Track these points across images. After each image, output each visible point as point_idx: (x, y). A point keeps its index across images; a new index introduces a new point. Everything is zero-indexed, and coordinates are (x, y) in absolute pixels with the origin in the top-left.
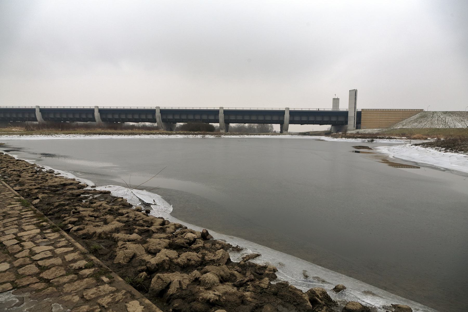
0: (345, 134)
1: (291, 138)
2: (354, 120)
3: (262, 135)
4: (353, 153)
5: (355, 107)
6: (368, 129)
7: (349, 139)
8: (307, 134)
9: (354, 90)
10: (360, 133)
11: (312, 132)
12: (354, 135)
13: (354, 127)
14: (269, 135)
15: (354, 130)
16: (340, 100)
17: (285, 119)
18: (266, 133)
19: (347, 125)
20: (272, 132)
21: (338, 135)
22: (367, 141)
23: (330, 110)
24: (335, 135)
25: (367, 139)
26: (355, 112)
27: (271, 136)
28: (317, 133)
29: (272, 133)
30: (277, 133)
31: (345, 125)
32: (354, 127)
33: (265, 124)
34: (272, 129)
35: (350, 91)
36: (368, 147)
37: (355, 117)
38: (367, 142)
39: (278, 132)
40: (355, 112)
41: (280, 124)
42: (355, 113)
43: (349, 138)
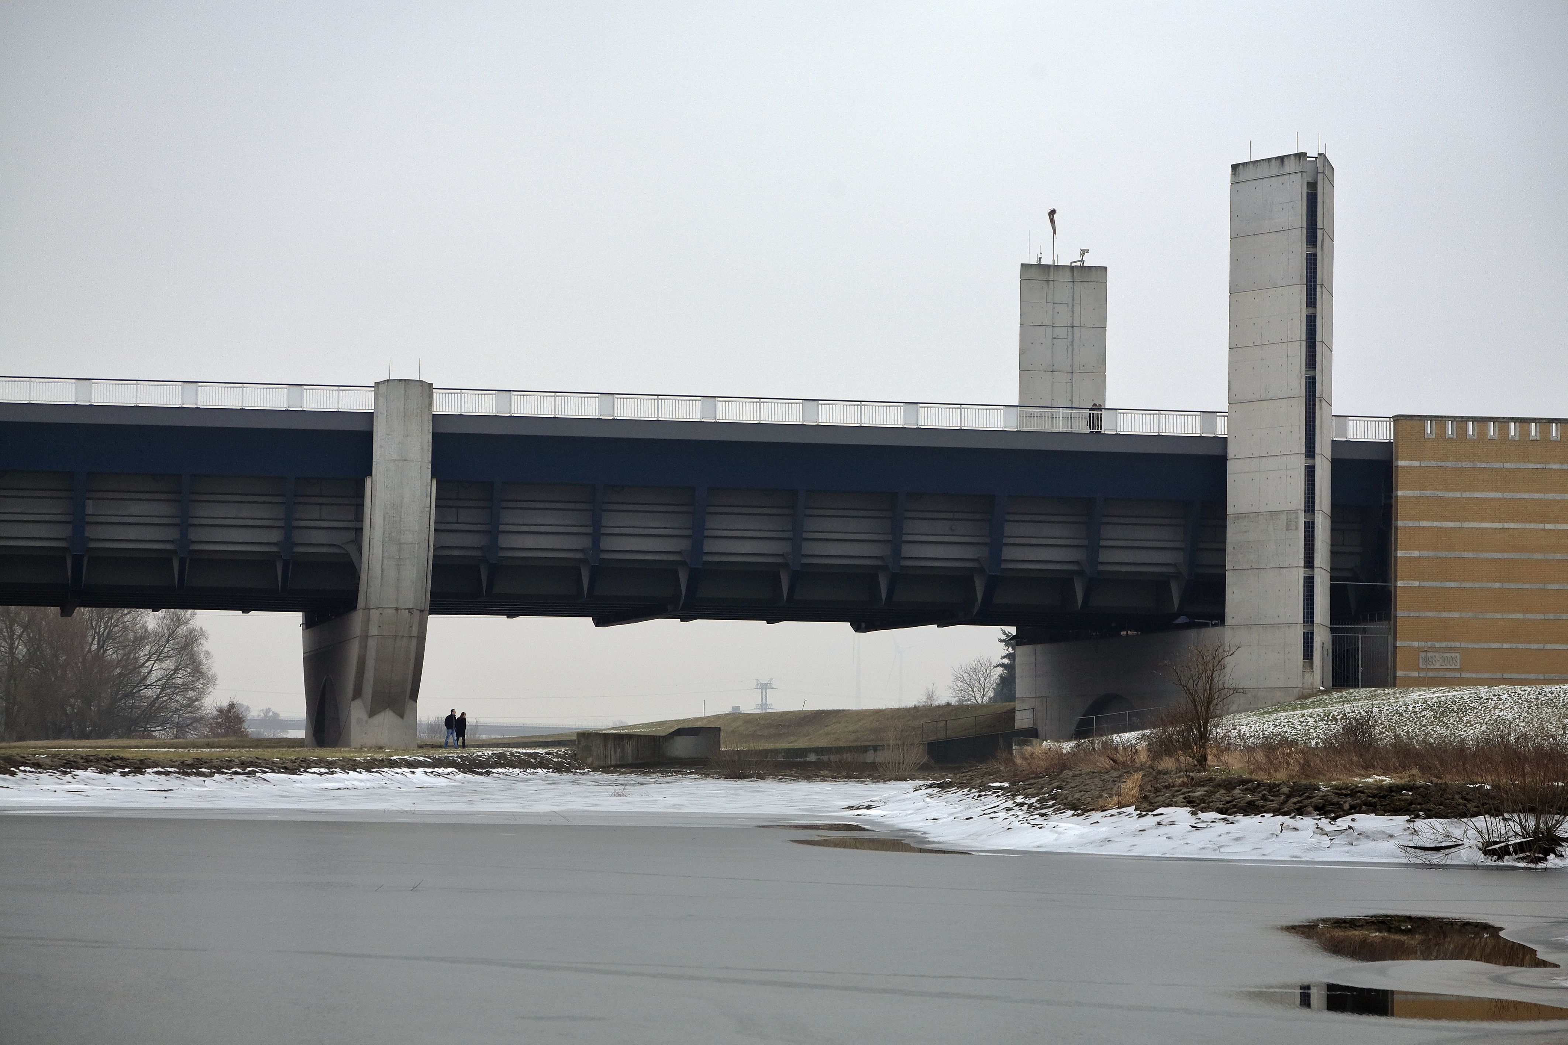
0: (1186, 747)
1: (459, 806)
2: (1309, 562)
3: (38, 766)
4: (1305, 1012)
5: (1311, 384)
6: (1483, 691)
7: (1246, 823)
8: (681, 748)
9: (1291, 166)
10: (1383, 736)
11: (750, 720)
12: (1306, 766)
13: (1308, 654)
14: (138, 767)
15: (1304, 697)
16: (1111, 277)
17: (378, 534)
18: (102, 746)
19: (1210, 633)
20: (181, 728)
21: (1104, 762)
22: (1468, 854)
23: (993, 421)
24: (1062, 763)
25: (1480, 822)
26: (1310, 451)
27: (172, 782)
28: (822, 743)
29: (192, 736)
30: (259, 743)
31: (1192, 633)
32: (1308, 654)
33: (84, 613)
34: (186, 687)
35: (1235, 167)
36: (1494, 931)
37: (1310, 528)
38: (1480, 858)
39: (273, 720)
40: (1310, 451)
41: (297, 618)
42: (1310, 472)
43: (1251, 809)
